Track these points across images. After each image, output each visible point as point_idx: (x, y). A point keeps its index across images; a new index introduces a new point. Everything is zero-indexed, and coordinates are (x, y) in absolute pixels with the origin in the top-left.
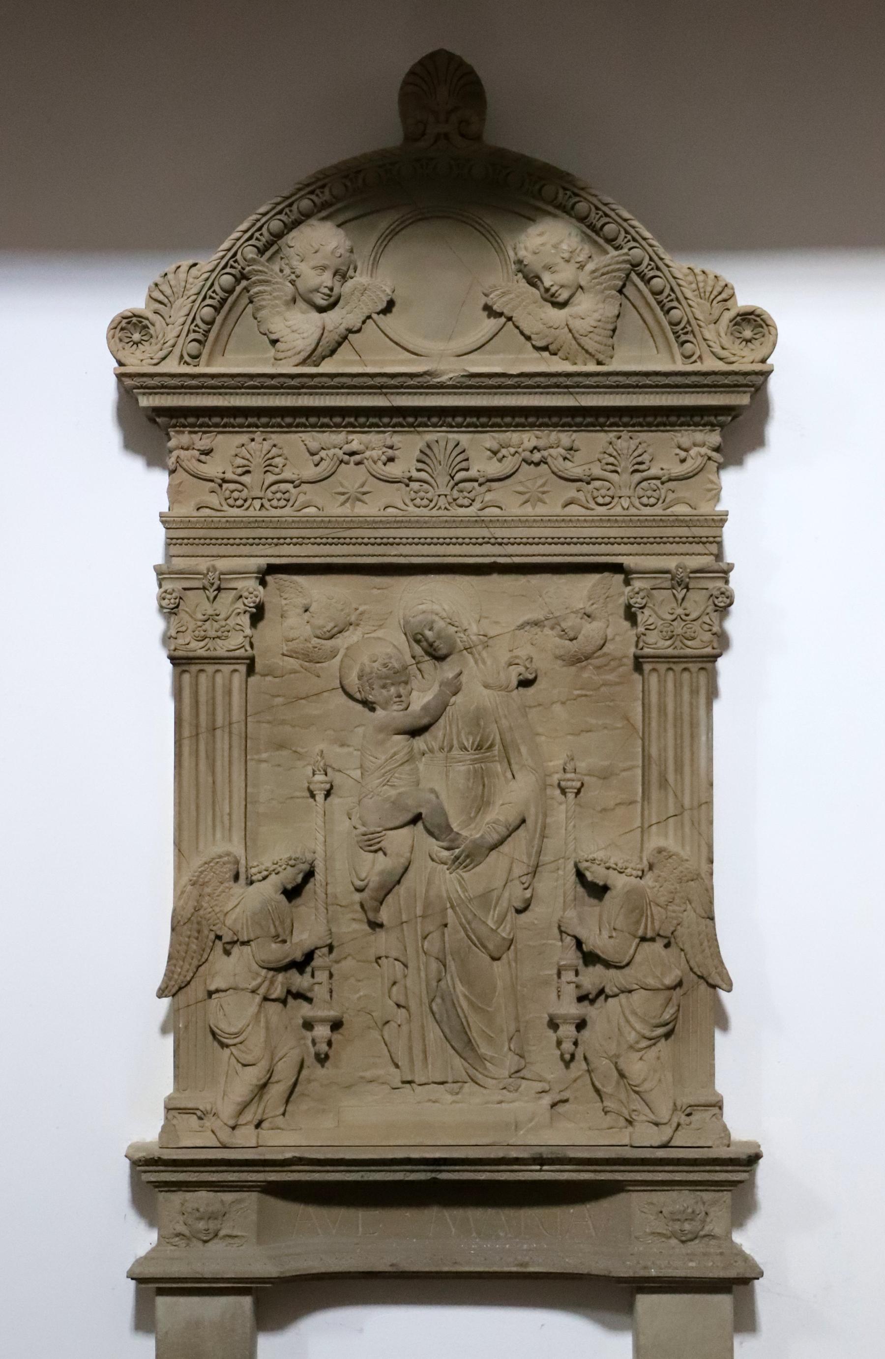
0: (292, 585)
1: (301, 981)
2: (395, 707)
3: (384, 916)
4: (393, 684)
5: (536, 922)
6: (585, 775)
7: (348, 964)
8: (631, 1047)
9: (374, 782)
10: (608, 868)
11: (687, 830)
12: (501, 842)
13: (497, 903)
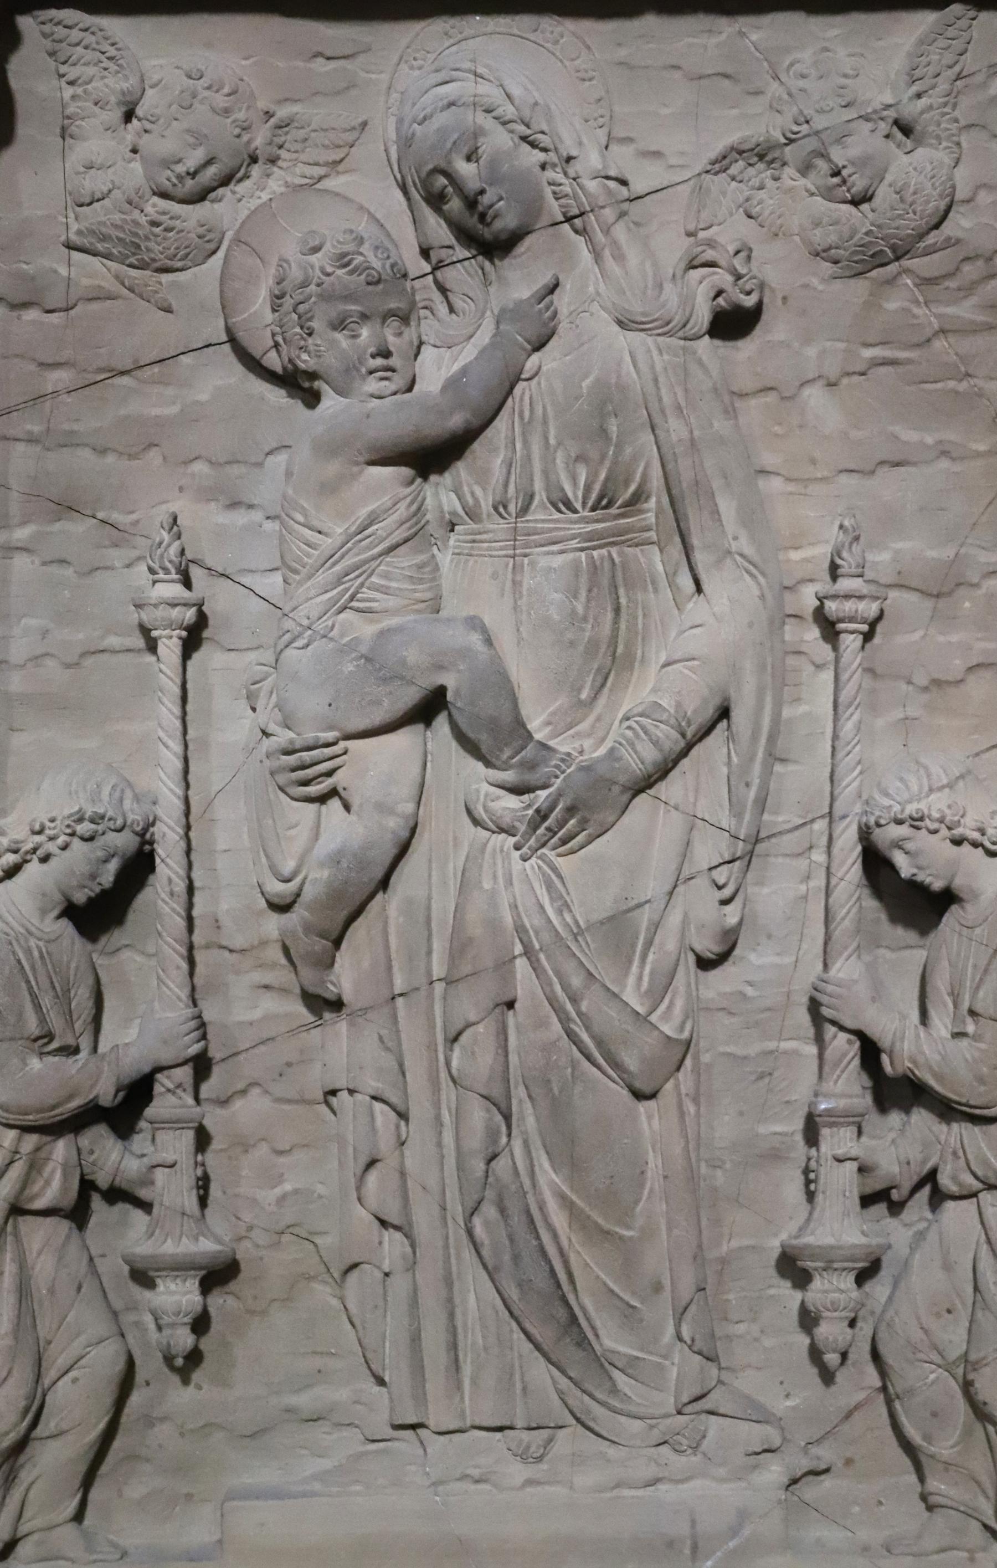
0: (89, 39)
1: (110, 1156)
2: (372, 385)
3: (346, 977)
4: (364, 317)
5: (750, 991)
6: (890, 586)
7: (249, 1111)
9: (311, 601)
10: (957, 842)
12: (664, 771)
13: (649, 944)
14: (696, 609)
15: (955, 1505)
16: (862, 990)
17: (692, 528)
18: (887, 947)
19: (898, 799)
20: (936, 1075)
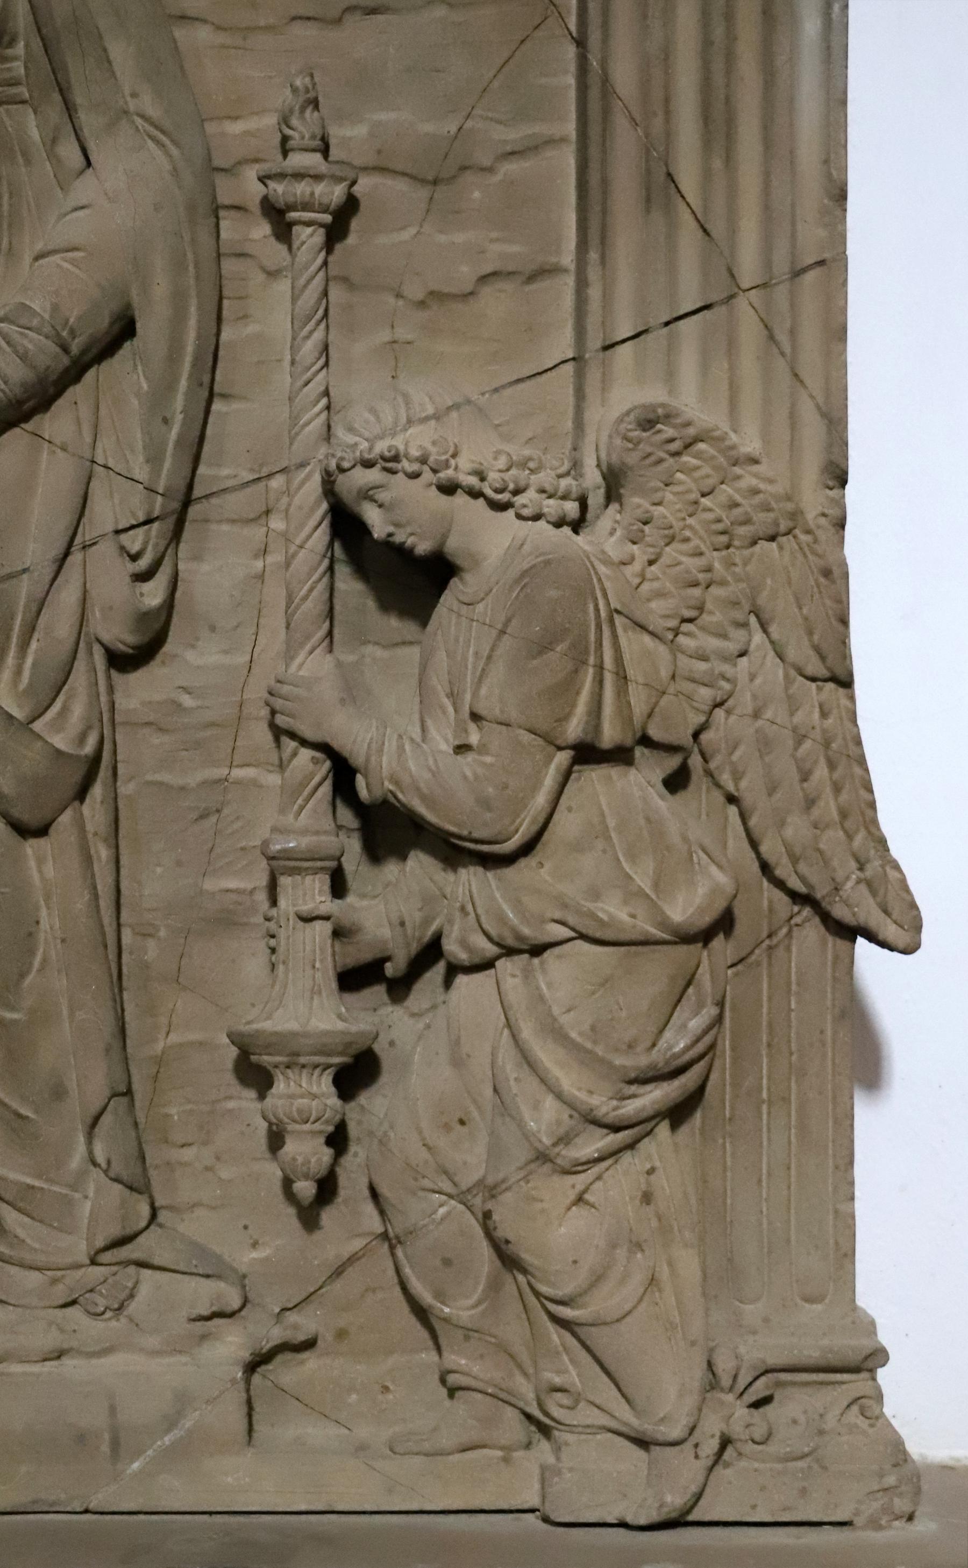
5: (187, 701)
8: (542, 1157)
10: (449, 489)
11: (748, 364)
13: (30, 629)
14: (86, 189)
15: (479, 1385)
16: (329, 691)
17: (73, 81)
18: (376, 643)
19: (367, 434)
20: (423, 798)
